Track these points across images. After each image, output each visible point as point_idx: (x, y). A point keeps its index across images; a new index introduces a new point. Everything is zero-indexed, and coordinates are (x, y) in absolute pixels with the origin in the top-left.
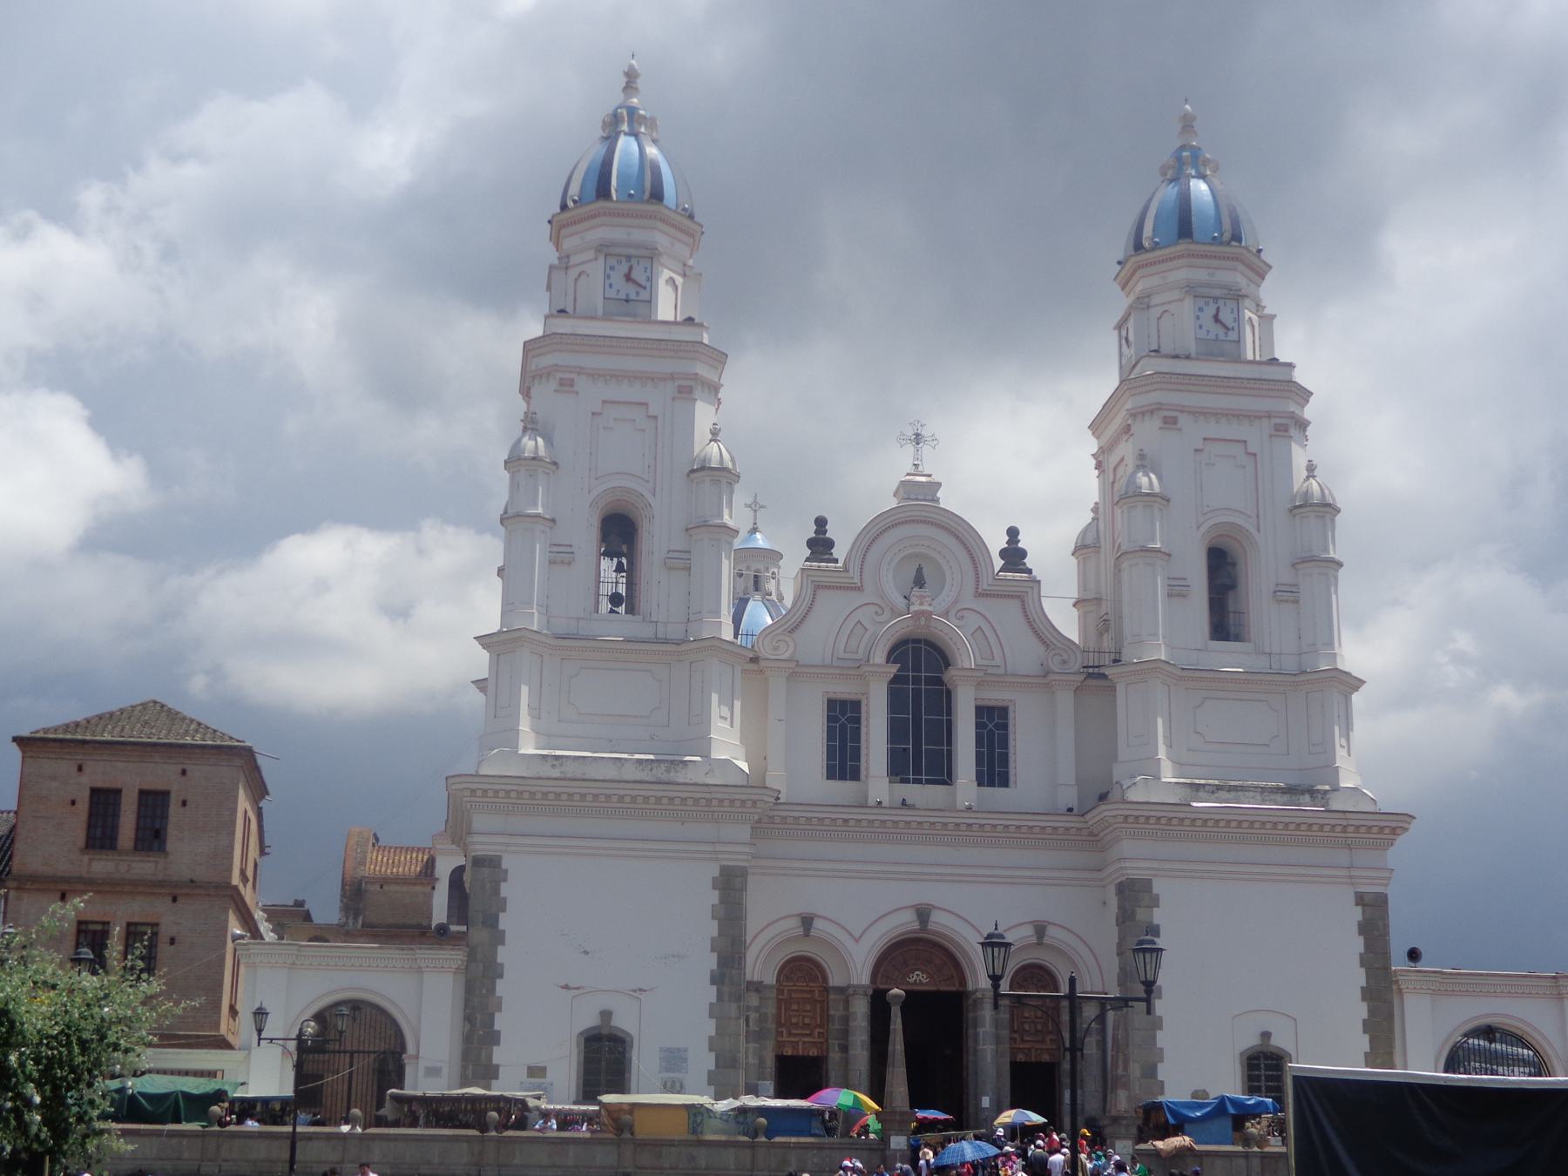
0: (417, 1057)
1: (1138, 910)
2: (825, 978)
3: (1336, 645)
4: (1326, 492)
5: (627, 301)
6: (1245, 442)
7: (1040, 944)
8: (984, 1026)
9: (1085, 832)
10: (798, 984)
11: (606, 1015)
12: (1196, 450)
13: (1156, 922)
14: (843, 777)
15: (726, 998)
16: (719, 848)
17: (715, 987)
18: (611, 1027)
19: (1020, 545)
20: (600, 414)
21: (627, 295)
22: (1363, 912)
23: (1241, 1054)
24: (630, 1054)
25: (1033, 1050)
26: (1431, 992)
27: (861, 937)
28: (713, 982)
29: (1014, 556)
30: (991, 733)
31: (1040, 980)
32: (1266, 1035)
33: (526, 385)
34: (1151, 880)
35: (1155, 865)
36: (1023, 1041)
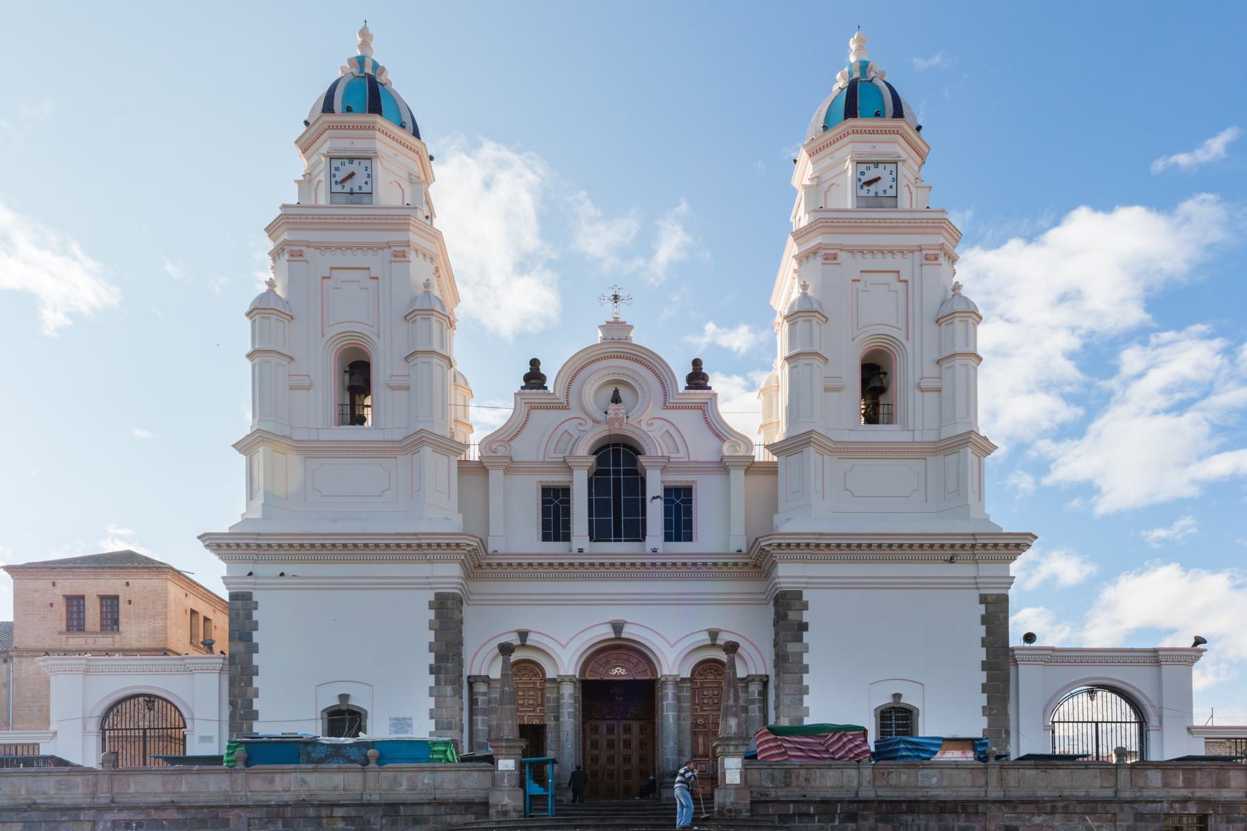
2: (544, 674)
5: (351, 193)
8: (668, 700)
12: (854, 281)
13: (805, 620)
14: (557, 539)
15: (442, 683)
17: (433, 676)
18: (348, 705)
21: (351, 189)
24: (365, 722)
26: (1043, 663)
28: (431, 673)
32: (897, 696)
34: (801, 591)
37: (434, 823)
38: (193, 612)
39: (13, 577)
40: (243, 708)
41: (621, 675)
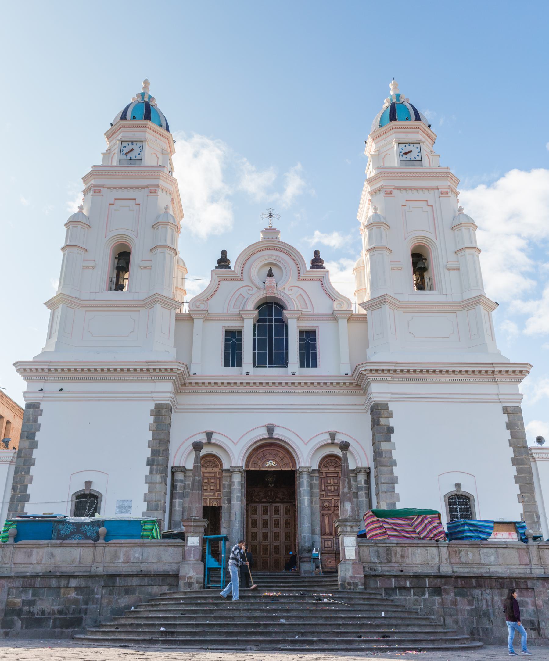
1: (381, 419)
2: (222, 466)
5: (131, 160)
10: (208, 469)
11: (88, 484)
12: (402, 205)
14: (233, 366)
15: (154, 472)
17: (149, 467)
24: (100, 504)
25: (333, 500)
27: (308, 442)
28: (148, 464)
30: (308, 344)
31: (335, 463)
32: (88, 484)
36: (327, 495)
37: (139, 593)
41: (272, 466)
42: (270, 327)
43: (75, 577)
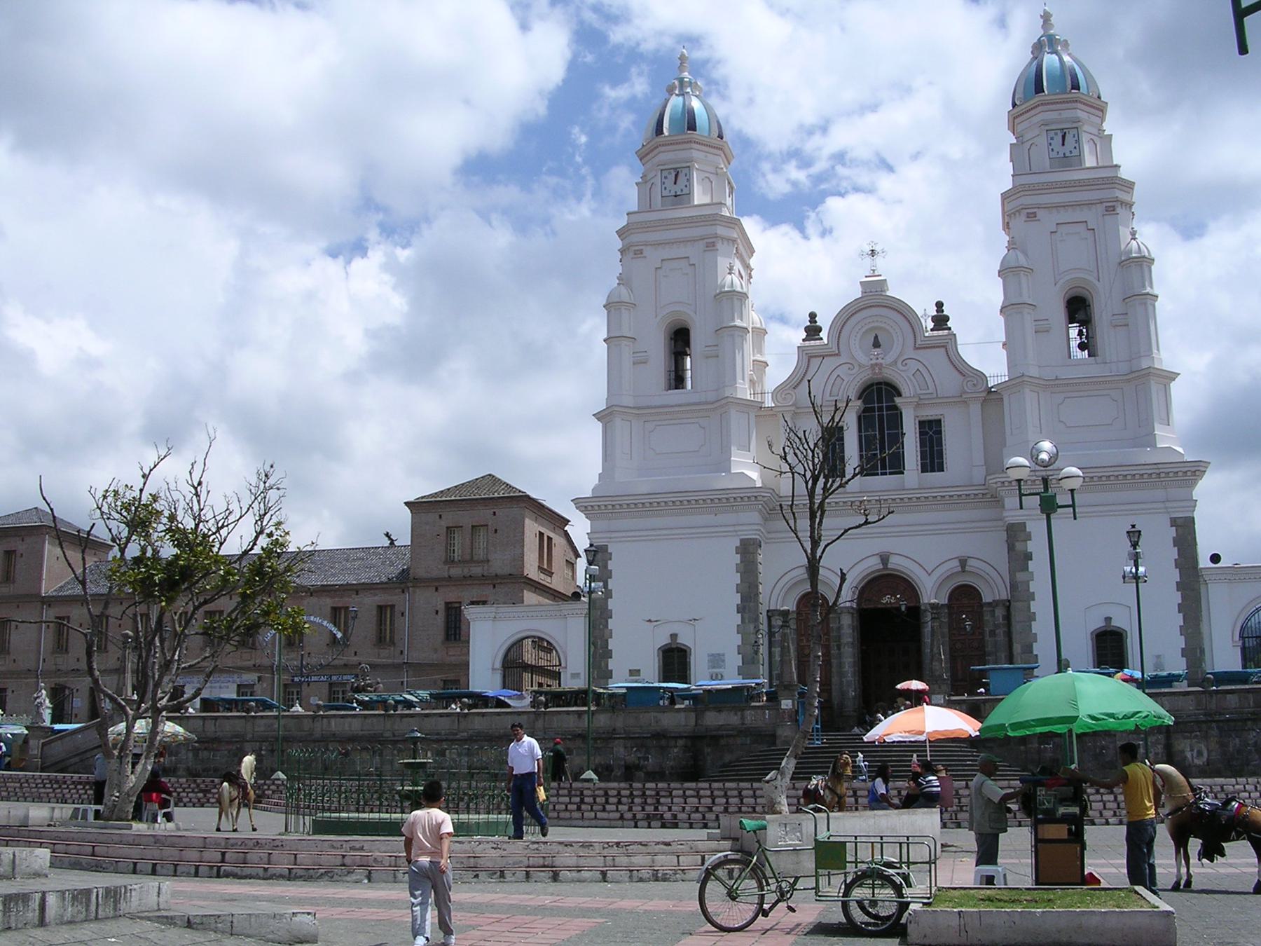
0: (566, 668)
1: (1017, 544)
3: (1155, 351)
4: (1141, 246)
5: (676, 196)
6: (1086, 222)
7: (963, 571)
9: (989, 496)
11: (674, 636)
15: (747, 621)
16: (737, 528)
19: (945, 313)
20: (1055, 232)
22: (1177, 530)
23: (1092, 633)
29: (941, 321)
32: (1108, 619)
33: (1006, 221)
35: (608, 535)
38: (540, 533)
39: (412, 513)
40: (602, 648)
42: (881, 417)
43: (681, 737)
